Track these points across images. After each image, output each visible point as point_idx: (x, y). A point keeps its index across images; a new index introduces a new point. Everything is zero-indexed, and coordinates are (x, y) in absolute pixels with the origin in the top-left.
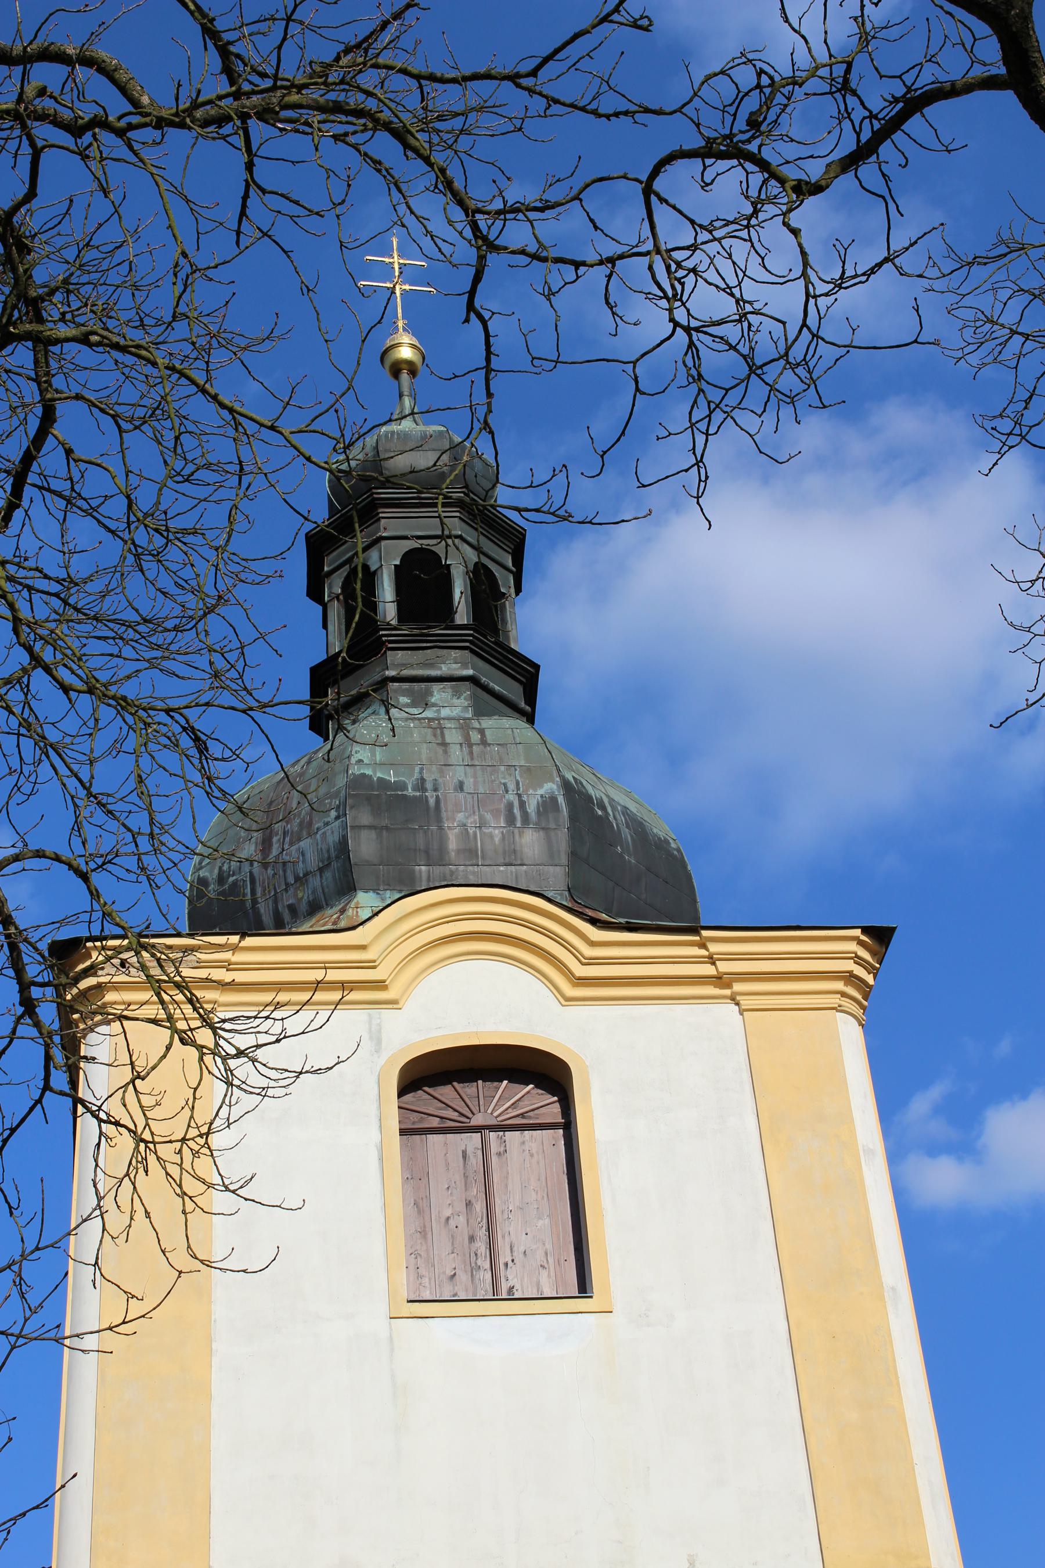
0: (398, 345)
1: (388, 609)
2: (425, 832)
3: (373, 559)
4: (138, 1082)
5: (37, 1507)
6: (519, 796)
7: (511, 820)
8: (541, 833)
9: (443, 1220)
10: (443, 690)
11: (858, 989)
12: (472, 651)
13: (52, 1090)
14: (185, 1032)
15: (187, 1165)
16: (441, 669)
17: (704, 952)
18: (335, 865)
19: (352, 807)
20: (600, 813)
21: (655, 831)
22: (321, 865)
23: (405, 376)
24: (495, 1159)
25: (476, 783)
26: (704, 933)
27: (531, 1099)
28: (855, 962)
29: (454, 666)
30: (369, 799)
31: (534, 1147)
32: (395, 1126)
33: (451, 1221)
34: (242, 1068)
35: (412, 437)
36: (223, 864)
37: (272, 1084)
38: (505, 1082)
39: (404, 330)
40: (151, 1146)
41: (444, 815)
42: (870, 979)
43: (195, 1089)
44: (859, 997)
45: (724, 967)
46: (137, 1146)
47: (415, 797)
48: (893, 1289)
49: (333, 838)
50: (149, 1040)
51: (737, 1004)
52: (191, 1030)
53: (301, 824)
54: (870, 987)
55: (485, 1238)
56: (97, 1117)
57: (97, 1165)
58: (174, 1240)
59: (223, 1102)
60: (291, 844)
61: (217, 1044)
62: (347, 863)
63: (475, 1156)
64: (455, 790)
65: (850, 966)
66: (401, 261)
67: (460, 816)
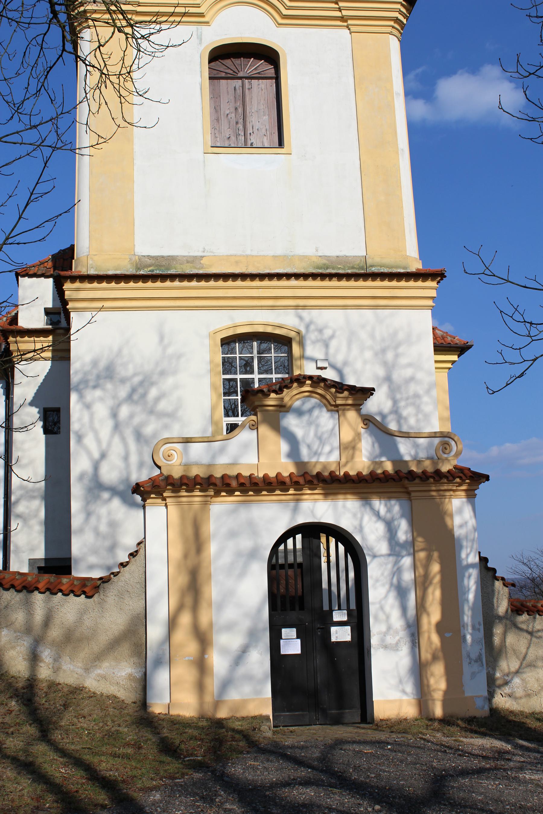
4: (101, 47)
5: (66, 212)
9: (226, 115)
11: (399, 25)
13: (66, 51)
14: (120, 27)
15: (122, 84)
17: (337, 6)
24: (247, 91)
27: (262, 66)
28: (399, 13)
31: (263, 86)
32: (206, 75)
33: (229, 116)
34: (144, 44)
37: (157, 51)
38: (252, 59)
40: (107, 76)
42: (405, 21)
43: (125, 51)
44: (400, 29)
45: (345, 13)
46: (101, 76)
48: (402, 150)
50: (105, 32)
51: (349, 29)
52: (123, 27)
54: (405, 25)
55: (242, 123)
56: (85, 63)
57: (86, 84)
58: (117, 114)
59: (136, 57)
61: (133, 33)
63: (239, 89)
65: (397, 15)
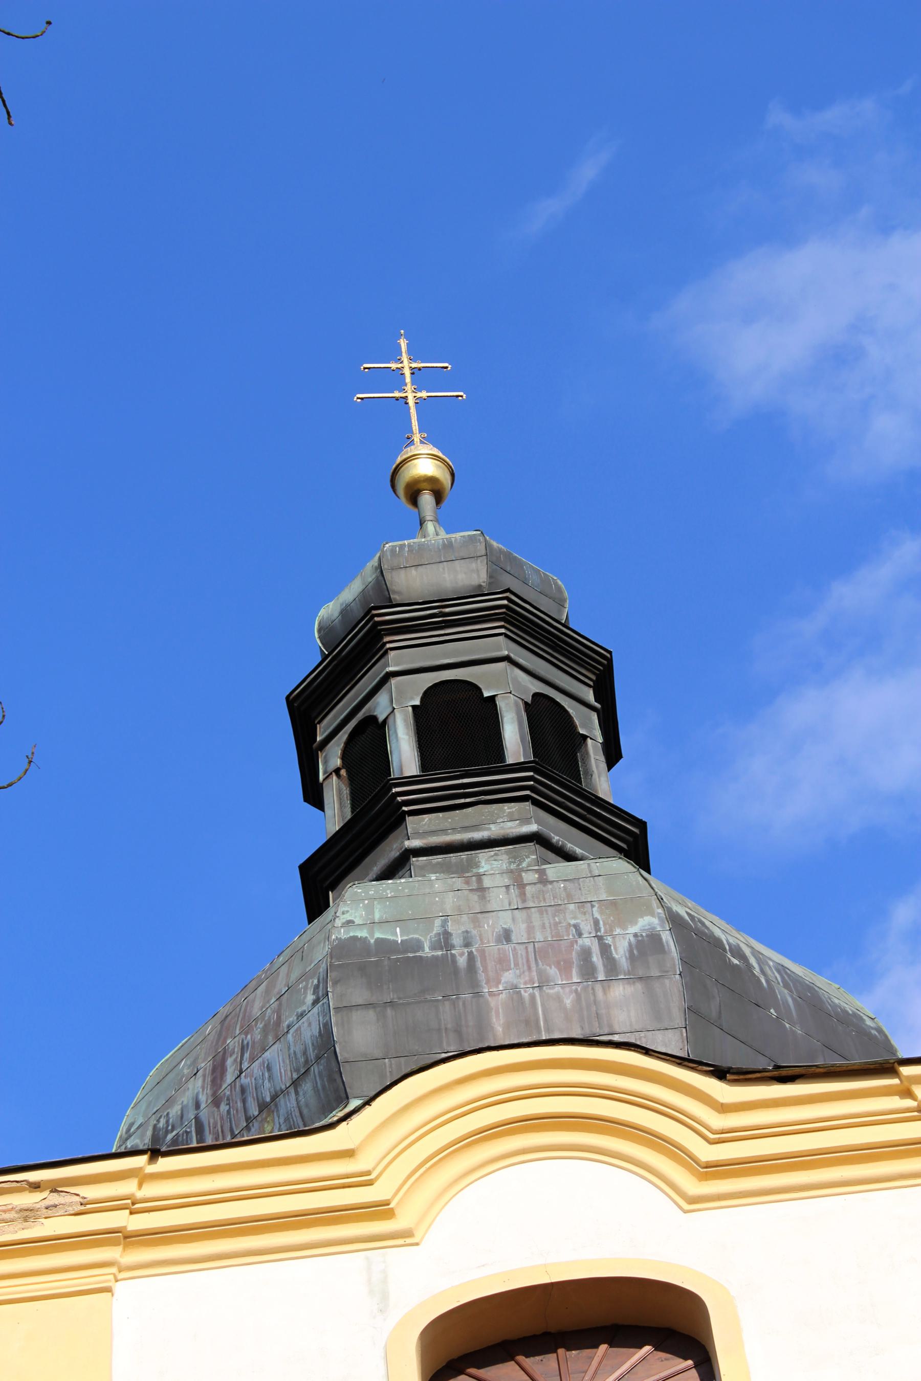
0: (414, 457)
1: (404, 754)
2: (454, 1003)
3: (380, 706)
6: (600, 939)
7: (588, 971)
8: (639, 986)
10: (495, 858)
12: (536, 803)
16: (490, 829)
17: (909, 1103)
18: (315, 1069)
19: (335, 983)
20: (736, 961)
21: (836, 1001)
22: (295, 1076)
23: (427, 499)
25: (530, 930)
26: (905, 1071)
29: (510, 824)
30: (362, 969)
35: (437, 562)
36: (158, 1121)
39: (421, 442)
41: (482, 976)
47: (436, 958)
49: (309, 1030)
53: (265, 1031)
60: (252, 1060)
62: (334, 1064)
64: (498, 941)
66: (414, 365)
67: (508, 977)
